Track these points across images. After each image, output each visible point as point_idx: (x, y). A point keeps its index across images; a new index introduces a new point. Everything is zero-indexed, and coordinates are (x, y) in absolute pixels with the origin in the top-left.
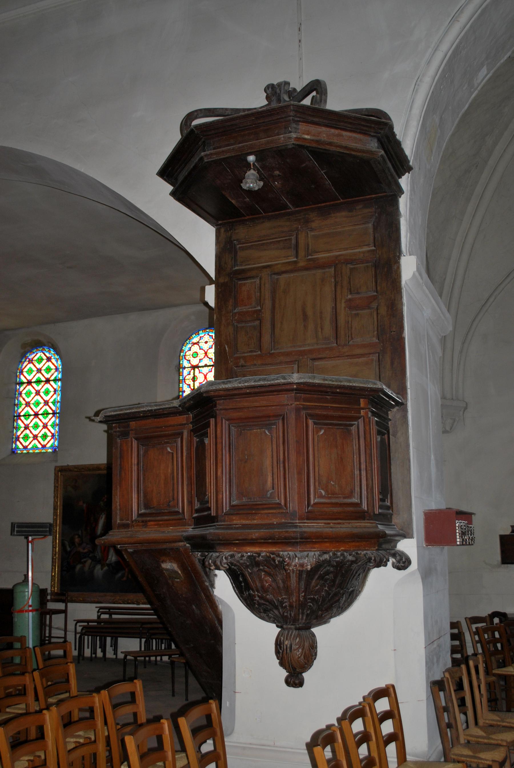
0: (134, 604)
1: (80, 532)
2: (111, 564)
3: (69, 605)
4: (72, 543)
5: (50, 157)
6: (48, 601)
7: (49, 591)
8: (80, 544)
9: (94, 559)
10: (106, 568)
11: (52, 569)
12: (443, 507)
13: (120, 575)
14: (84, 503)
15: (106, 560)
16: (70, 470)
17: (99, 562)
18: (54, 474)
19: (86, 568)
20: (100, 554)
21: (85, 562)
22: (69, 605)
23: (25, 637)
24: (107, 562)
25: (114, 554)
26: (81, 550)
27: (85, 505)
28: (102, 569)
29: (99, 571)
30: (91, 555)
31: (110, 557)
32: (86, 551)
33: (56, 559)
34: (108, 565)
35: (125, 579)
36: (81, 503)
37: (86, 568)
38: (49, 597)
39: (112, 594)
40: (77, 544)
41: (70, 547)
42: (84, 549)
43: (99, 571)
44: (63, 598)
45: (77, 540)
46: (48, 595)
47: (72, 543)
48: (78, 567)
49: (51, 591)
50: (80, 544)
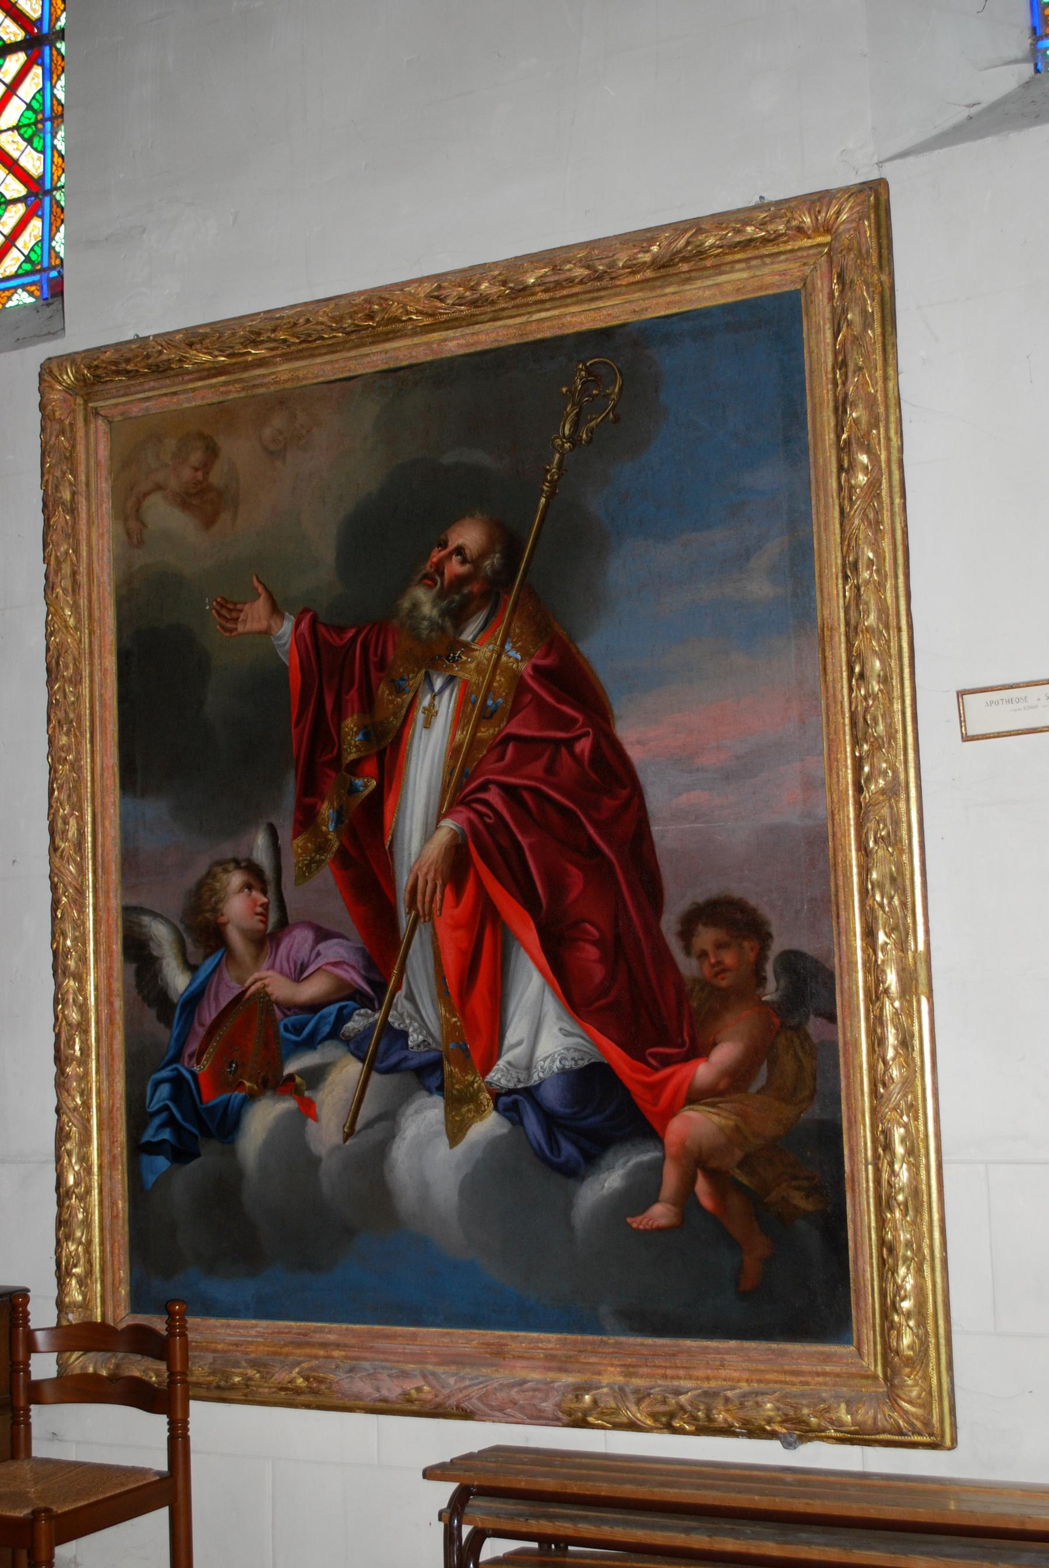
0: (754, 1431)
1: (261, 840)
2: (530, 1093)
3: (202, 1415)
4: (205, 933)
5: (115, 712)
6: (37, 1393)
7: (42, 1315)
8: (264, 941)
9: (382, 1051)
10: (488, 1125)
11: (61, 1136)
12: (154, 1157)
13: (611, 1179)
14: (276, 610)
15: (487, 1066)
16: (161, 370)
17: (428, 1074)
18: (36, 416)
19: (326, 1132)
20: (431, 1013)
21: (316, 1076)
22: (202, 1415)
23: (404, 690)
24: (499, 1075)
25: (552, 1007)
26: (281, 988)
27: (285, 629)
28: (455, 1132)
29: (432, 1153)
30: (356, 1023)
31: (517, 1030)
32: (312, 989)
33: (84, 1061)
34: (513, 1102)
35: (660, 1213)
36: (255, 615)
37: (326, 1132)
38: (43, 1366)
39: (550, 1340)
40: (234, 937)
41: (191, 968)
42: (299, 974)
43: (432, 1153)
44: (149, 1370)
45: (238, 907)
46: (32, 1348)
47: (205, 933)
48: (263, 1118)
49: (61, 1304)
50: (264, 941)
